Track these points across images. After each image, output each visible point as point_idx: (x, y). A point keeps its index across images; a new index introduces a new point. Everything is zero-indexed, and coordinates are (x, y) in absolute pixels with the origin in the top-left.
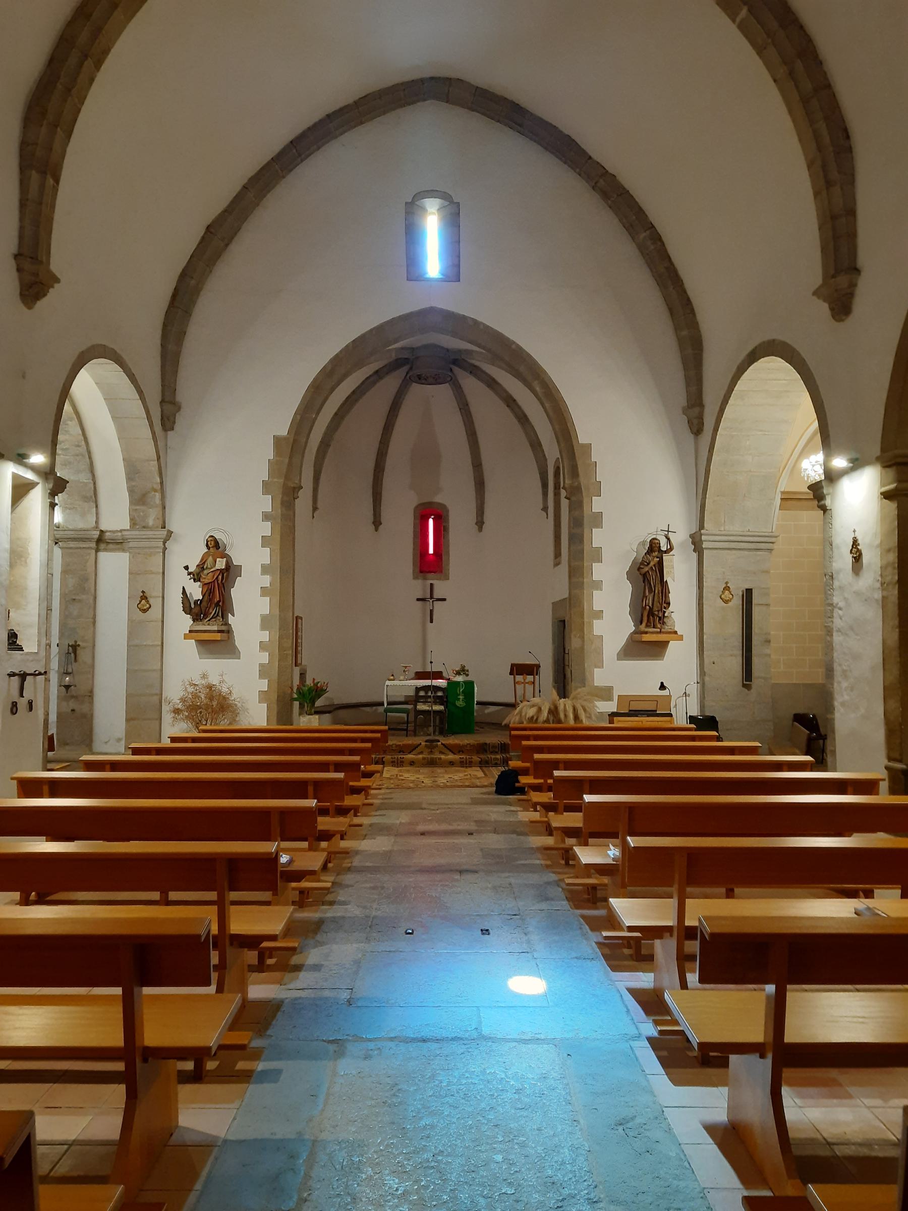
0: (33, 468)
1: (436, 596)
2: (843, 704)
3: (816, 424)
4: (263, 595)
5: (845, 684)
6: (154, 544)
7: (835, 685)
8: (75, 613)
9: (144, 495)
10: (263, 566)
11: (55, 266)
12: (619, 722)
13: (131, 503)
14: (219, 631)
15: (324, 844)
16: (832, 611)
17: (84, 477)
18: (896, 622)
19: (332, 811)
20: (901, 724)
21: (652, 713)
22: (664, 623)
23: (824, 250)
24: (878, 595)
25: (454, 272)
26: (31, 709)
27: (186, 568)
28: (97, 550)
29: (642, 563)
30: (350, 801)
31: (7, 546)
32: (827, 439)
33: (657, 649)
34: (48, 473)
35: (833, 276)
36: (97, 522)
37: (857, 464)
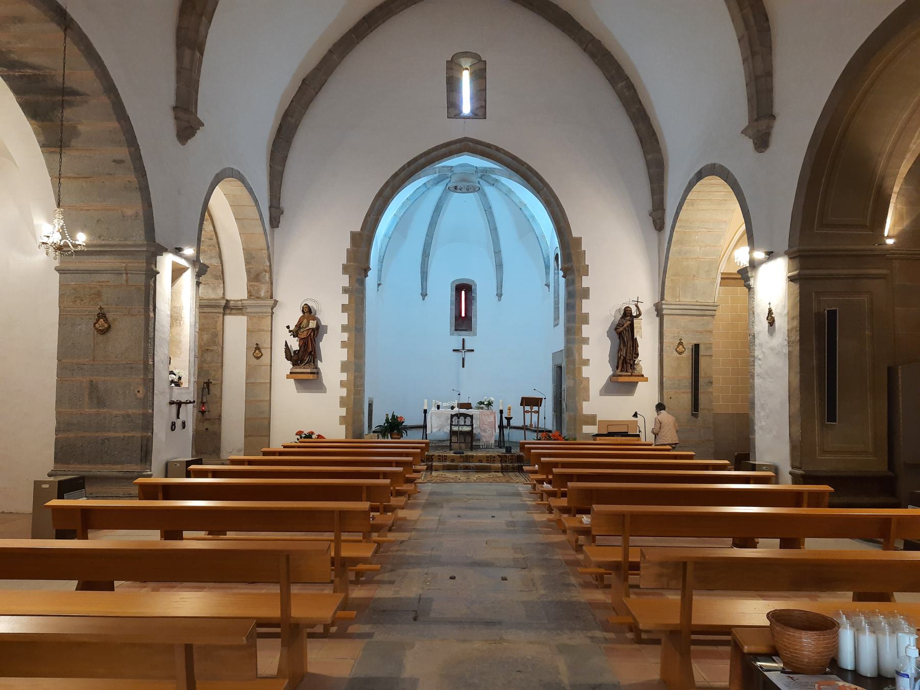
0: (186, 258)
1: (467, 348)
2: (761, 428)
3: (744, 227)
4: (342, 347)
5: (762, 414)
6: (264, 310)
7: (756, 414)
8: (209, 359)
9: (258, 275)
10: (343, 326)
11: (201, 115)
12: (599, 440)
13: (248, 280)
14: (311, 373)
15: (375, 536)
16: (754, 361)
17: (215, 262)
18: (798, 369)
19: (381, 509)
20: (801, 442)
21: (625, 434)
22: (634, 369)
23: (749, 100)
24: (786, 350)
25: (480, 111)
26: (184, 427)
27: (288, 327)
28: (224, 314)
29: (618, 325)
30: (394, 501)
31: (169, 313)
32: (751, 238)
33: (629, 388)
34: (195, 262)
35: (756, 120)
36: (224, 294)
37: (770, 255)
